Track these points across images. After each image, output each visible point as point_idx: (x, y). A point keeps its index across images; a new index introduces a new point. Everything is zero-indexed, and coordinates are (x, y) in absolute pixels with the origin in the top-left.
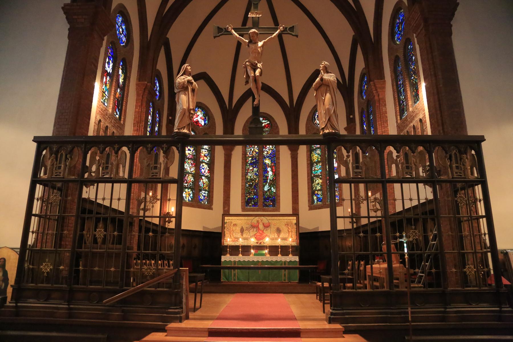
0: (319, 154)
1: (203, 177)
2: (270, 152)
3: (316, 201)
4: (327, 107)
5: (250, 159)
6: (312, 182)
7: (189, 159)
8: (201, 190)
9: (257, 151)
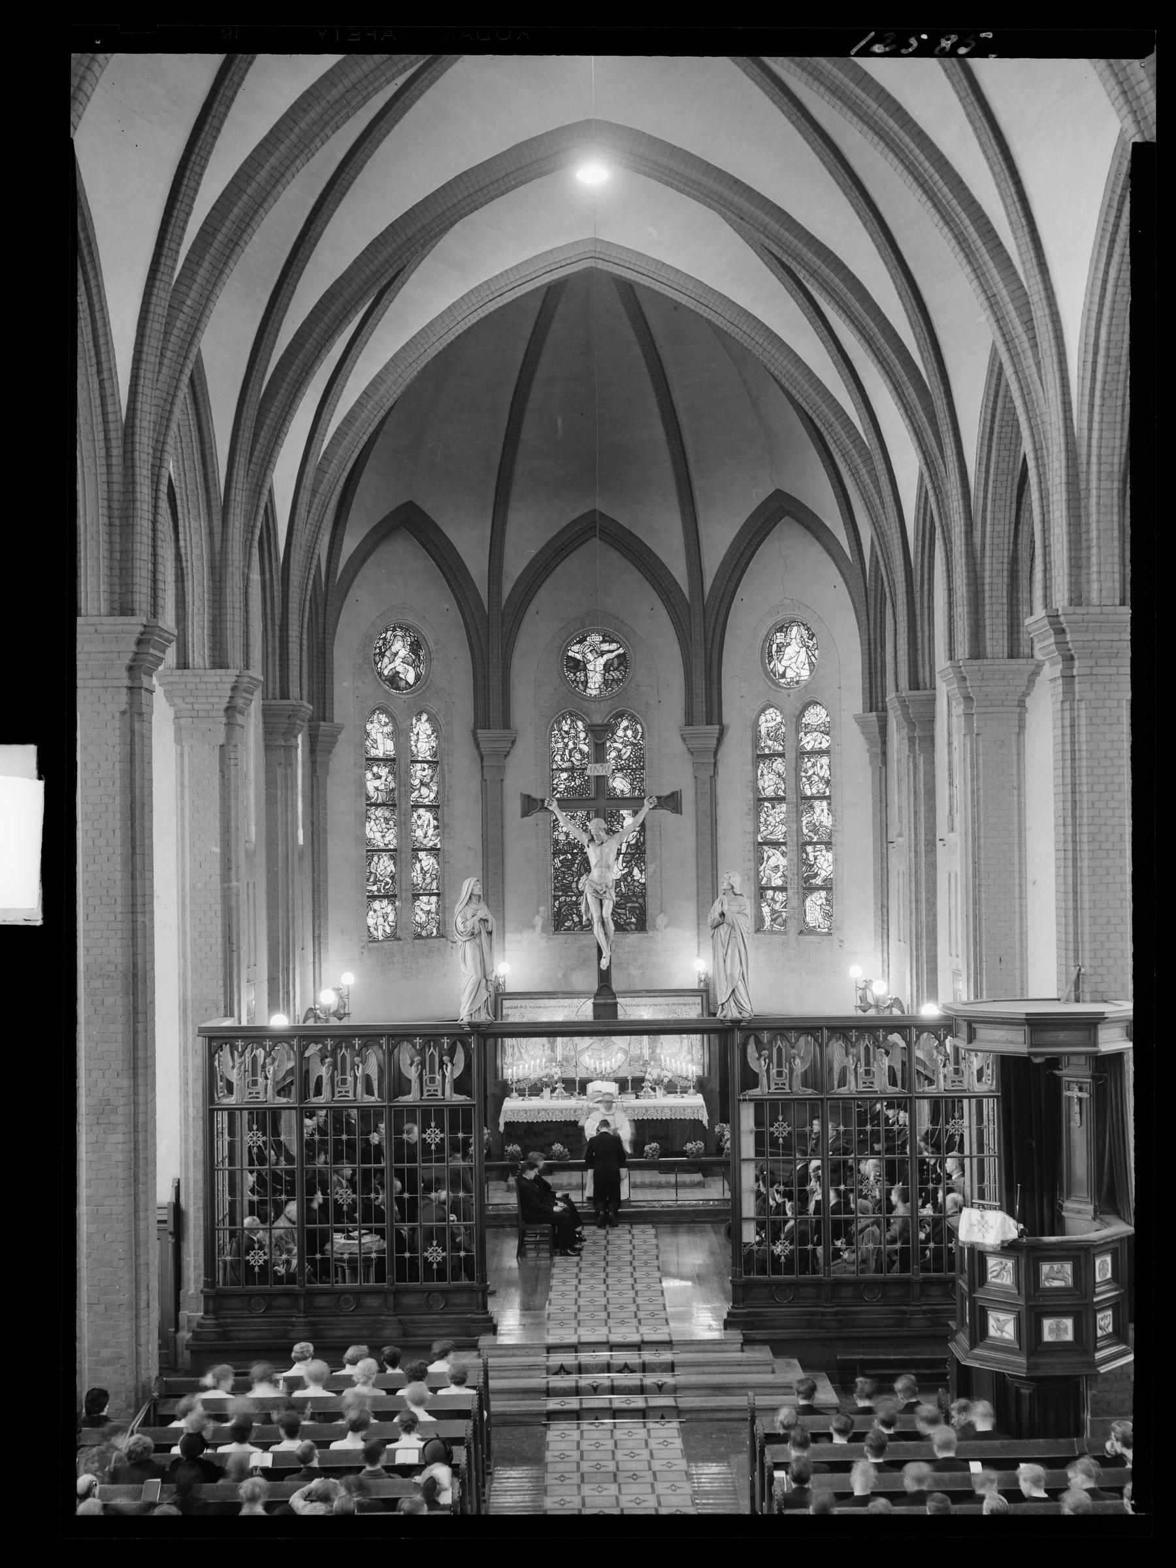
0: (779, 775)
1: (422, 855)
3: (768, 919)
4: (292, 1270)
5: (564, 775)
6: (760, 860)
7: (377, 805)
8: (416, 897)
9: (586, 749)
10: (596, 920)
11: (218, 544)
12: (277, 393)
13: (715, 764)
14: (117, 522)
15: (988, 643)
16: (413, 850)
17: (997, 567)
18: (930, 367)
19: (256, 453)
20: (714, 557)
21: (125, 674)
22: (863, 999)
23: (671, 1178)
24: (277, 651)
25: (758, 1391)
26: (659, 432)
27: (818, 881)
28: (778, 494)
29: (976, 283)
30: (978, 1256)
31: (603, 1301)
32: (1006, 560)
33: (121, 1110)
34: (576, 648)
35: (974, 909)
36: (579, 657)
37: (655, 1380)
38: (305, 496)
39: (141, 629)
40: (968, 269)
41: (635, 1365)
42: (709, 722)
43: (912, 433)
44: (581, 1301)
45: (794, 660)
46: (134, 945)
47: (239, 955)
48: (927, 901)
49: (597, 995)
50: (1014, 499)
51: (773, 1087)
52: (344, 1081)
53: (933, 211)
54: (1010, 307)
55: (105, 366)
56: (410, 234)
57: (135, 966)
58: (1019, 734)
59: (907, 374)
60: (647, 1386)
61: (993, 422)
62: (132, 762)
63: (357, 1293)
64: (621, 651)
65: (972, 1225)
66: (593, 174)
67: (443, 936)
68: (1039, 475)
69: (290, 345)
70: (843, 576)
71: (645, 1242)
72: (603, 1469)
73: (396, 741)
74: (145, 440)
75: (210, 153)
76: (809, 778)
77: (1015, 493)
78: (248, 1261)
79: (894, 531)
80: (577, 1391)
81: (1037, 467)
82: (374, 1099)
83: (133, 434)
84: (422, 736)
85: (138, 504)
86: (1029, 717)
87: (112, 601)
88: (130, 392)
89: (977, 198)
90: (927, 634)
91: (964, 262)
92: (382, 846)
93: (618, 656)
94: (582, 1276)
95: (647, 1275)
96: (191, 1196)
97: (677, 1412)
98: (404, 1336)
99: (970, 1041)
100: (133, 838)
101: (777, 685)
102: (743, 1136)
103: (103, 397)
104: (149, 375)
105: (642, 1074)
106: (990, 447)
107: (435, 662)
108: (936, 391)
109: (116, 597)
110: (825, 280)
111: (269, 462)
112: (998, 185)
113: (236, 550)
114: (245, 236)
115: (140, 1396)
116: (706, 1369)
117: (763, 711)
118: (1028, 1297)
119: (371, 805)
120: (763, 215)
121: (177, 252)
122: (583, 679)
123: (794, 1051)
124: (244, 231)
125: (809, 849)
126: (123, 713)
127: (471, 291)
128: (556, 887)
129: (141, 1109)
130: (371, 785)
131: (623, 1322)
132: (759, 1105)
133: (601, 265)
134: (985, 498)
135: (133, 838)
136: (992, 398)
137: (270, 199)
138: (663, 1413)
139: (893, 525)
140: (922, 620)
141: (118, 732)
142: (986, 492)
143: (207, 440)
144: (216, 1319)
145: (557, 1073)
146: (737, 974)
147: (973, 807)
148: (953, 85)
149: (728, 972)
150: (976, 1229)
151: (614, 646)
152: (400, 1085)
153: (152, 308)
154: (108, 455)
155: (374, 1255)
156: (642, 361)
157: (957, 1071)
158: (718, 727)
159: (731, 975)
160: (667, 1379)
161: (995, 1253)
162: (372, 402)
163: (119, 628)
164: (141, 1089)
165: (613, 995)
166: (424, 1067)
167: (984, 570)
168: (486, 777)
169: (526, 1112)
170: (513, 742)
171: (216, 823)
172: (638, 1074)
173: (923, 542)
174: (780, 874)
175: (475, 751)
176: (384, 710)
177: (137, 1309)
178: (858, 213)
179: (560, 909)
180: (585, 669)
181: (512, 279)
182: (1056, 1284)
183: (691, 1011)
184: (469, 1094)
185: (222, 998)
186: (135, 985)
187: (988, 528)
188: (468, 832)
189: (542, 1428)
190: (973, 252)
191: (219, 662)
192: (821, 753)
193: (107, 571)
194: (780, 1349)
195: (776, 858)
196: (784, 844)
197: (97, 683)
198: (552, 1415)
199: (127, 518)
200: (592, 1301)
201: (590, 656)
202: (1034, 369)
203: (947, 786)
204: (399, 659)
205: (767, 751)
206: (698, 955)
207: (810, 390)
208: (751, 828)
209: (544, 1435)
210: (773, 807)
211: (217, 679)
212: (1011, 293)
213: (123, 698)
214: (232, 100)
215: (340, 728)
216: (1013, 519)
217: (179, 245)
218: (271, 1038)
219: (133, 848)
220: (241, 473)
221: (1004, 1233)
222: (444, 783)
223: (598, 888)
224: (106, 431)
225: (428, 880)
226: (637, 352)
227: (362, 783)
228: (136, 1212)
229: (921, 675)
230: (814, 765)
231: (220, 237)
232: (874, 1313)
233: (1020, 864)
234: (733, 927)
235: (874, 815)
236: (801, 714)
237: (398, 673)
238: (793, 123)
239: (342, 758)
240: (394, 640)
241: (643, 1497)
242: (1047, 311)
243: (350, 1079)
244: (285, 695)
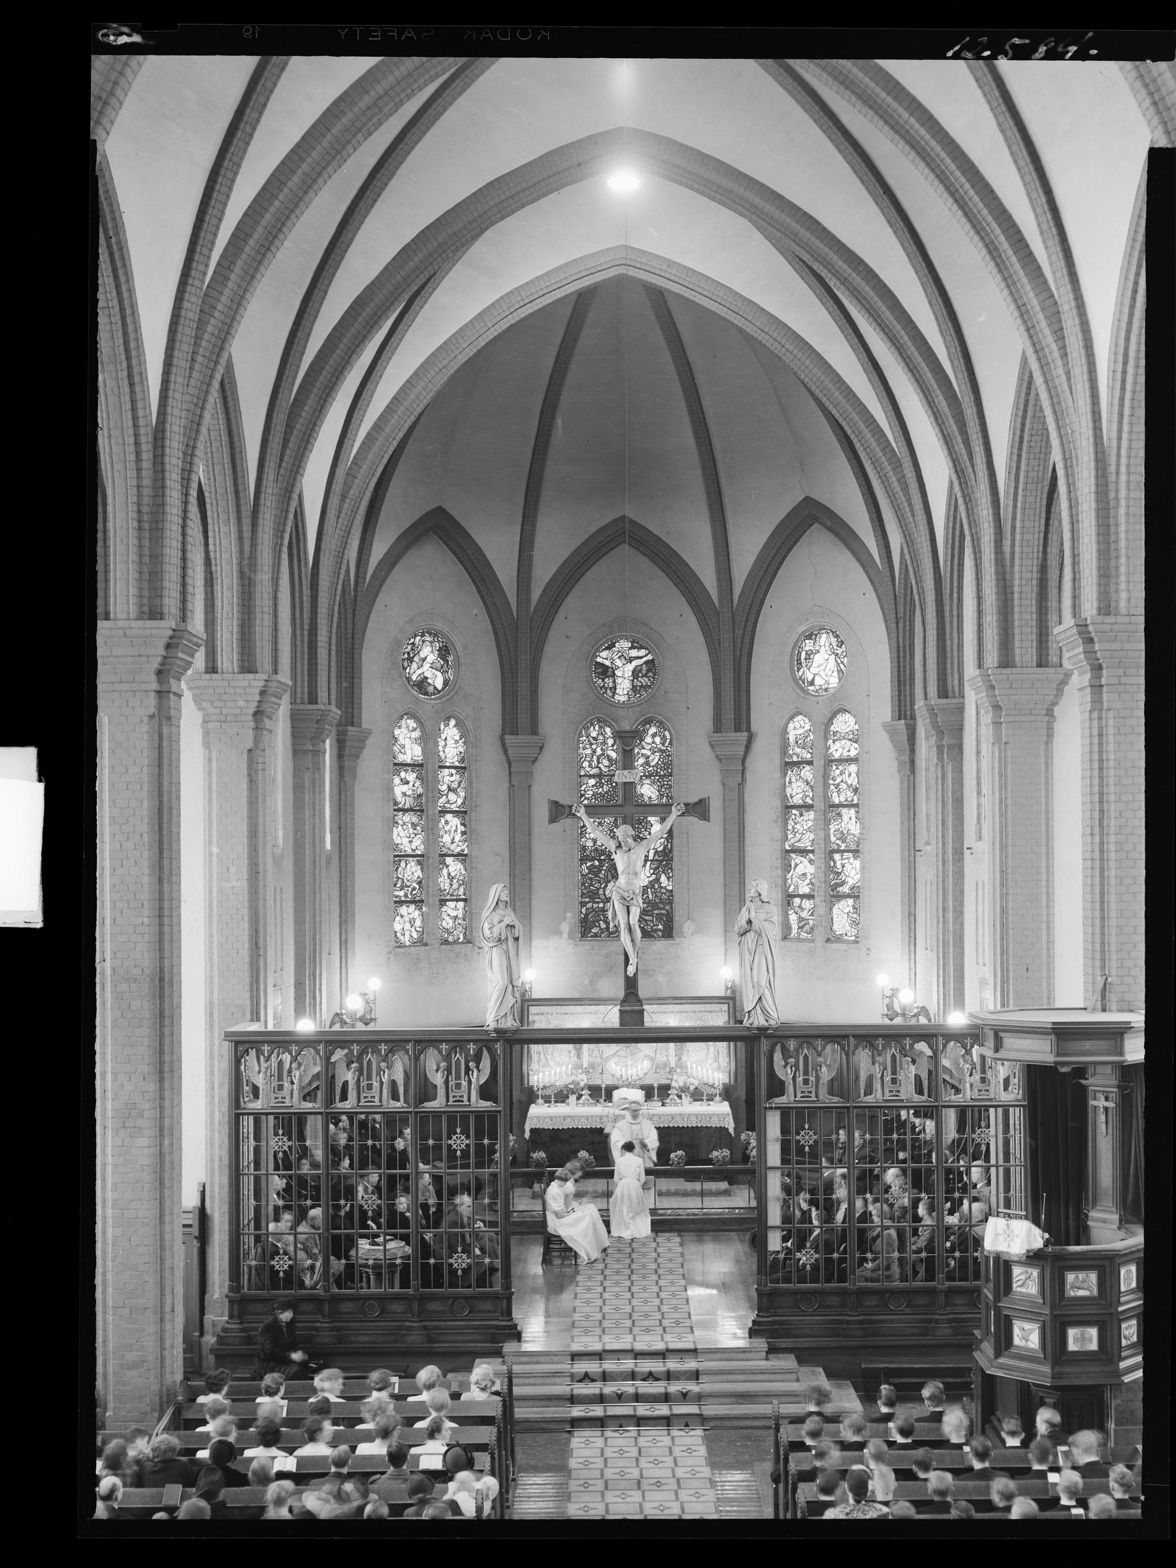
1: (449, 860)
2: (655, 759)
5: (592, 782)
6: (787, 868)
7: (405, 811)
8: (443, 902)
9: (613, 755)
10: (623, 927)
11: (247, 548)
12: (307, 398)
13: (743, 771)
14: (146, 526)
15: (1017, 651)
16: (441, 855)
17: (1027, 576)
18: (960, 376)
19: (286, 458)
20: (743, 564)
21: (154, 678)
22: (890, 1007)
23: (697, 1186)
24: (306, 656)
25: (782, 1399)
26: (690, 440)
27: (845, 889)
28: (808, 501)
29: (1006, 292)
30: (1004, 1266)
31: (628, 1309)
32: (1035, 569)
33: (146, 1114)
34: (604, 654)
35: (1001, 918)
36: (607, 663)
37: (679, 1388)
38: (334, 501)
39: (170, 633)
40: (999, 278)
41: (659, 1373)
42: (737, 729)
43: (942, 441)
44: (606, 1309)
45: (822, 668)
46: (161, 949)
47: (266, 959)
48: (955, 910)
49: (623, 1002)
50: (1044, 508)
51: (799, 1095)
52: (370, 1087)
53: (964, 220)
54: (1041, 316)
55: (136, 370)
56: (440, 240)
57: (161, 970)
58: (1047, 743)
59: (937, 382)
60: (658, 1393)
61: (1022, 430)
62: (160, 766)
63: (382, 1299)
64: (650, 657)
65: (997, 1234)
66: (624, 181)
67: (469, 942)
68: (1069, 485)
69: (320, 351)
70: (872, 583)
71: (670, 1250)
72: (627, 1476)
73: (425, 744)
74: (175, 444)
75: (242, 159)
76: (837, 786)
77: (1044, 502)
78: (273, 1266)
79: (923, 538)
80: (601, 1399)
81: (1067, 475)
82: (399, 1105)
83: (163, 438)
84: (450, 742)
85: (168, 509)
86: (1058, 727)
87: (141, 606)
88: (161, 397)
89: (1008, 207)
90: (956, 642)
91: (995, 271)
92: (409, 852)
93: (647, 663)
94: (607, 1283)
95: (672, 1283)
96: (217, 1200)
97: (702, 1419)
98: (430, 1341)
99: (997, 1050)
100: (160, 842)
101: (806, 692)
102: (769, 1144)
103: (133, 402)
104: (180, 380)
105: (669, 1082)
106: (1019, 456)
107: (463, 668)
108: (966, 399)
109: (145, 601)
110: (855, 288)
111: (299, 467)
112: (1028, 195)
113: (265, 555)
114: (277, 242)
115: (165, 1400)
116: (731, 1377)
117: (792, 718)
118: (1053, 1307)
119: (399, 810)
120: (793, 224)
121: (209, 258)
122: (611, 685)
123: (821, 1059)
124: (275, 237)
125: (837, 857)
126: (152, 717)
127: (502, 298)
128: (583, 894)
129: (167, 1112)
130: (399, 790)
131: (647, 1330)
132: (785, 1113)
133: (632, 272)
134: (1015, 506)
135: (160, 842)
136: (1022, 407)
137: (302, 205)
138: (687, 1421)
139: (923, 533)
140: (952, 628)
141: (146, 737)
142: (1015, 500)
143: (237, 444)
144: (241, 1323)
145: (583, 1079)
146: (764, 982)
147: (1001, 815)
148: (985, 95)
149: (755, 980)
150: (1001, 1238)
151: (643, 652)
152: (426, 1091)
153: (183, 313)
154: (138, 459)
155: (398, 1261)
156: (672, 368)
157: (983, 1080)
158: (746, 734)
159: (758, 983)
160: (693, 1387)
161: (1019, 1263)
162: (402, 408)
163: (148, 632)
164: (167, 1094)
165: (640, 1002)
166: (449, 1073)
167: (1013, 579)
168: (514, 783)
169: (551, 1118)
170: (541, 748)
171: (244, 827)
172: (664, 1082)
173: (953, 549)
174: (807, 881)
175: (503, 758)
176: (411, 715)
177: (162, 1313)
178: (889, 222)
179: (586, 915)
180: (614, 675)
181: (543, 286)
182: (1081, 1293)
183: (718, 1018)
184: (495, 1100)
185: (248, 1002)
186: (162, 988)
187: (1018, 537)
188: (495, 839)
189: (567, 1435)
190: (1003, 261)
191: (248, 666)
192: (849, 760)
193: (136, 575)
194: (805, 1357)
195: (803, 866)
196: (812, 851)
197: (126, 686)
198: (576, 1423)
199: (157, 522)
200: (617, 1309)
201: (618, 663)
202: (1064, 378)
203: (975, 794)
204: (427, 665)
205: (795, 759)
206: (725, 963)
207: (841, 398)
208: (779, 836)
209: (568, 1442)
210: (801, 815)
211: (246, 683)
212: (1041, 302)
213: (152, 702)
214: (265, 105)
215: (368, 733)
216: (1043, 528)
217: (211, 250)
218: (297, 1042)
219: (161, 852)
220: (271, 477)
221: (1029, 1242)
222: (471, 788)
223: (626, 895)
224: (136, 436)
225: (455, 886)
226: (667, 358)
227: (390, 789)
228: (161, 1216)
229: (949, 683)
230: (842, 773)
231: (251, 242)
232: (899, 1321)
233: (1048, 873)
234: (760, 935)
235: (902, 823)
236: (830, 722)
237: (426, 678)
238: (824, 131)
239: (369, 764)
240: (422, 642)
241: (666, 1504)
242: (1077, 321)
243: (376, 1085)
244: (313, 700)
